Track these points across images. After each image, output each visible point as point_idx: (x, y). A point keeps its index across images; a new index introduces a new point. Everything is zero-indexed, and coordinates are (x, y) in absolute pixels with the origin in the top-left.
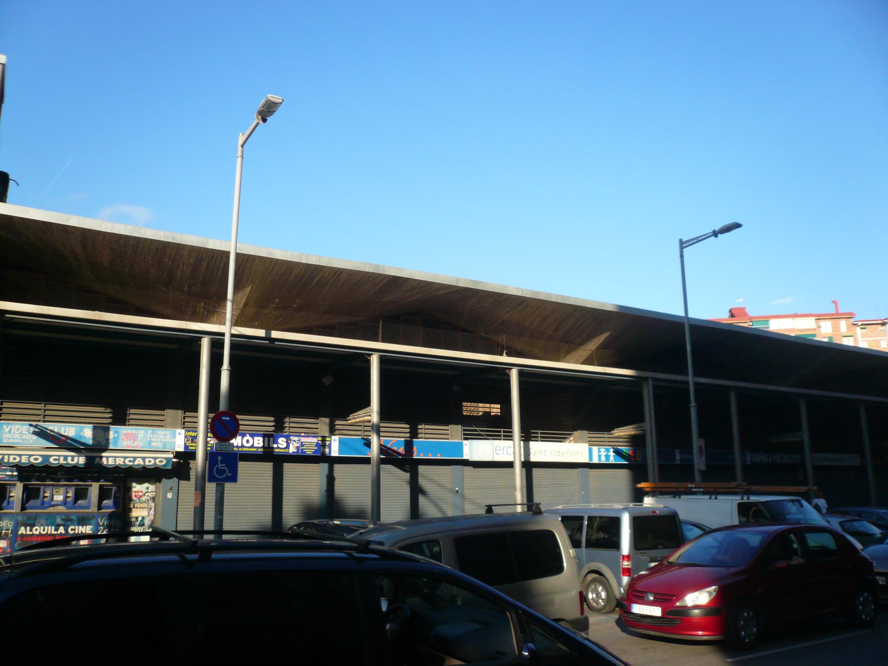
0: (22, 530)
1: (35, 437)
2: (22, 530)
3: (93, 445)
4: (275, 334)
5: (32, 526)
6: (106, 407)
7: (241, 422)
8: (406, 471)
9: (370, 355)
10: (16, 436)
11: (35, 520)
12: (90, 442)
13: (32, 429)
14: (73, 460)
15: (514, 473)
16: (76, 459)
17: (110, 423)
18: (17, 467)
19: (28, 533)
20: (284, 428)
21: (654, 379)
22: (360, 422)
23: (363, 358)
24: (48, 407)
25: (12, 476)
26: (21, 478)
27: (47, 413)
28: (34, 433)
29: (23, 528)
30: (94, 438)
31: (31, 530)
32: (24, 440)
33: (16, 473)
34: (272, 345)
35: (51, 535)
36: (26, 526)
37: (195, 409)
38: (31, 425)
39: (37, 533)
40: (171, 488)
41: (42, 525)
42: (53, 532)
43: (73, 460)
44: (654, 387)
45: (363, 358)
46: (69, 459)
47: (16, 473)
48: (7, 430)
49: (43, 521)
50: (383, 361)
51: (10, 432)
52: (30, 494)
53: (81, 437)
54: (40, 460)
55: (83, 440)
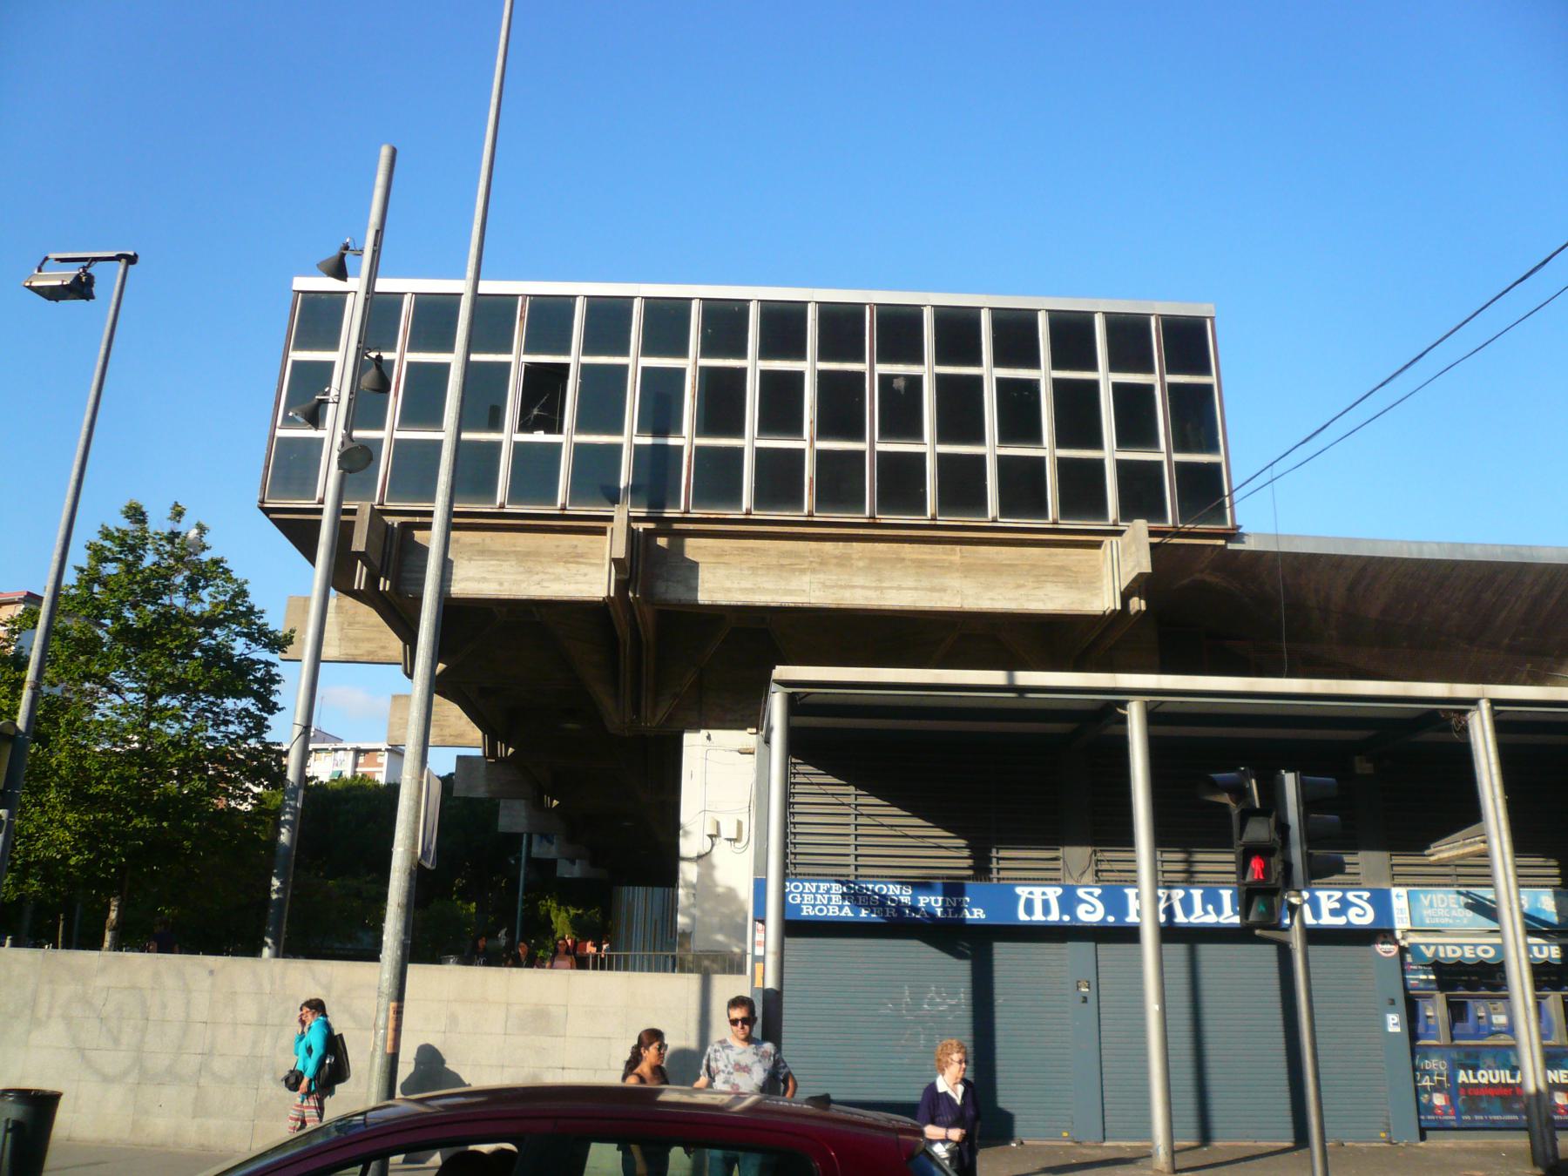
0: (1462, 1077)
1: (1470, 914)
2: (1462, 1077)
3: (1560, 924)
4: (1025, 678)
5: (1475, 1069)
6: (1547, 856)
7: (1232, 868)
8: (960, 955)
9: (1123, 704)
10: (1442, 912)
11: (1477, 1058)
12: (1555, 919)
13: (1463, 900)
14: (1541, 952)
15: (1139, 958)
16: (1545, 949)
17: (968, 878)
18: (1437, 966)
19: (1473, 1081)
20: (990, 871)
21: (1494, 702)
22: (1463, 857)
23: (1109, 711)
24: (1397, 860)
25: (1428, 981)
26: (1442, 985)
27: (861, 861)
28: (1468, 906)
29: (1462, 1073)
30: (1560, 912)
31: (1475, 1077)
32: (1455, 918)
33: (1432, 977)
34: (1021, 704)
35: (1507, 1085)
36: (1465, 1068)
37: (1125, 839)
38: (1459, 893)
39: (1484, 1081)
40: (1392, 1002)
41: (1489, 1068)
42: (1510, 1081)
43: (1541, 952)
44: (1495, 716)
45: (1109, 711)
46: (1535, 949)
47: (1432, 977)
48: (1426, 902)
49: (1490, 1061)
50: (1154, 717)
51: (1431, 906)
52: (1457, 1011)
53: (1539, 910)
54: (1492, 953)
55: (1543, 917)
